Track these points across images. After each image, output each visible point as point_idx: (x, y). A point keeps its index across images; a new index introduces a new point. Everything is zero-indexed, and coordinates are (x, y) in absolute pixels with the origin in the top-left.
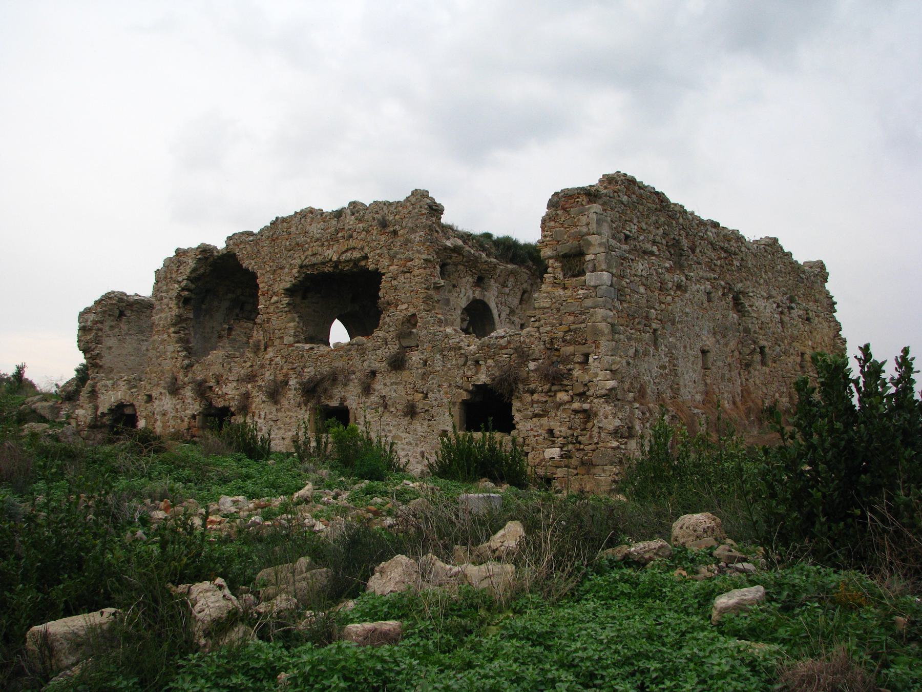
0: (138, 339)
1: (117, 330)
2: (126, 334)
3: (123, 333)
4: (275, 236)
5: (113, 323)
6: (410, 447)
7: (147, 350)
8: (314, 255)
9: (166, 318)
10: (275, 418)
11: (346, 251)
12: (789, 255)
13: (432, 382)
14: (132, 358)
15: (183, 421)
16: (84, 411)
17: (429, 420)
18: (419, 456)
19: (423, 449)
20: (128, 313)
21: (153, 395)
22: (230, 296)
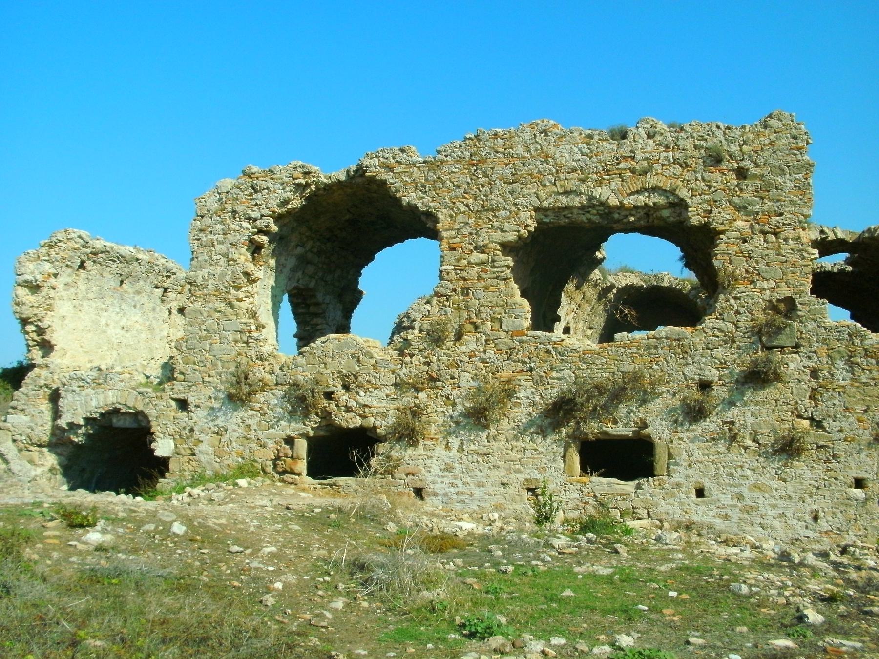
0: (96, 308)
1: (73, 290)
2: (84, 298)
3: (80, 296)
4: (476, 158)
5: (69, 280)
6: (788, 502)
7: (107, 325)
8: (566, 193)
9: (223, 275)
10: (484, 450)
11: (638, 192)
12: (360, 275)
13: (832, 403)
14: (90, 336)
15: (264, 446)
16: (27, 419)
17: (828, 461)
18: (808, 518)
19: (816, 507)
20: (89, 264)
21: (191, 400)
22: (299, 250)
